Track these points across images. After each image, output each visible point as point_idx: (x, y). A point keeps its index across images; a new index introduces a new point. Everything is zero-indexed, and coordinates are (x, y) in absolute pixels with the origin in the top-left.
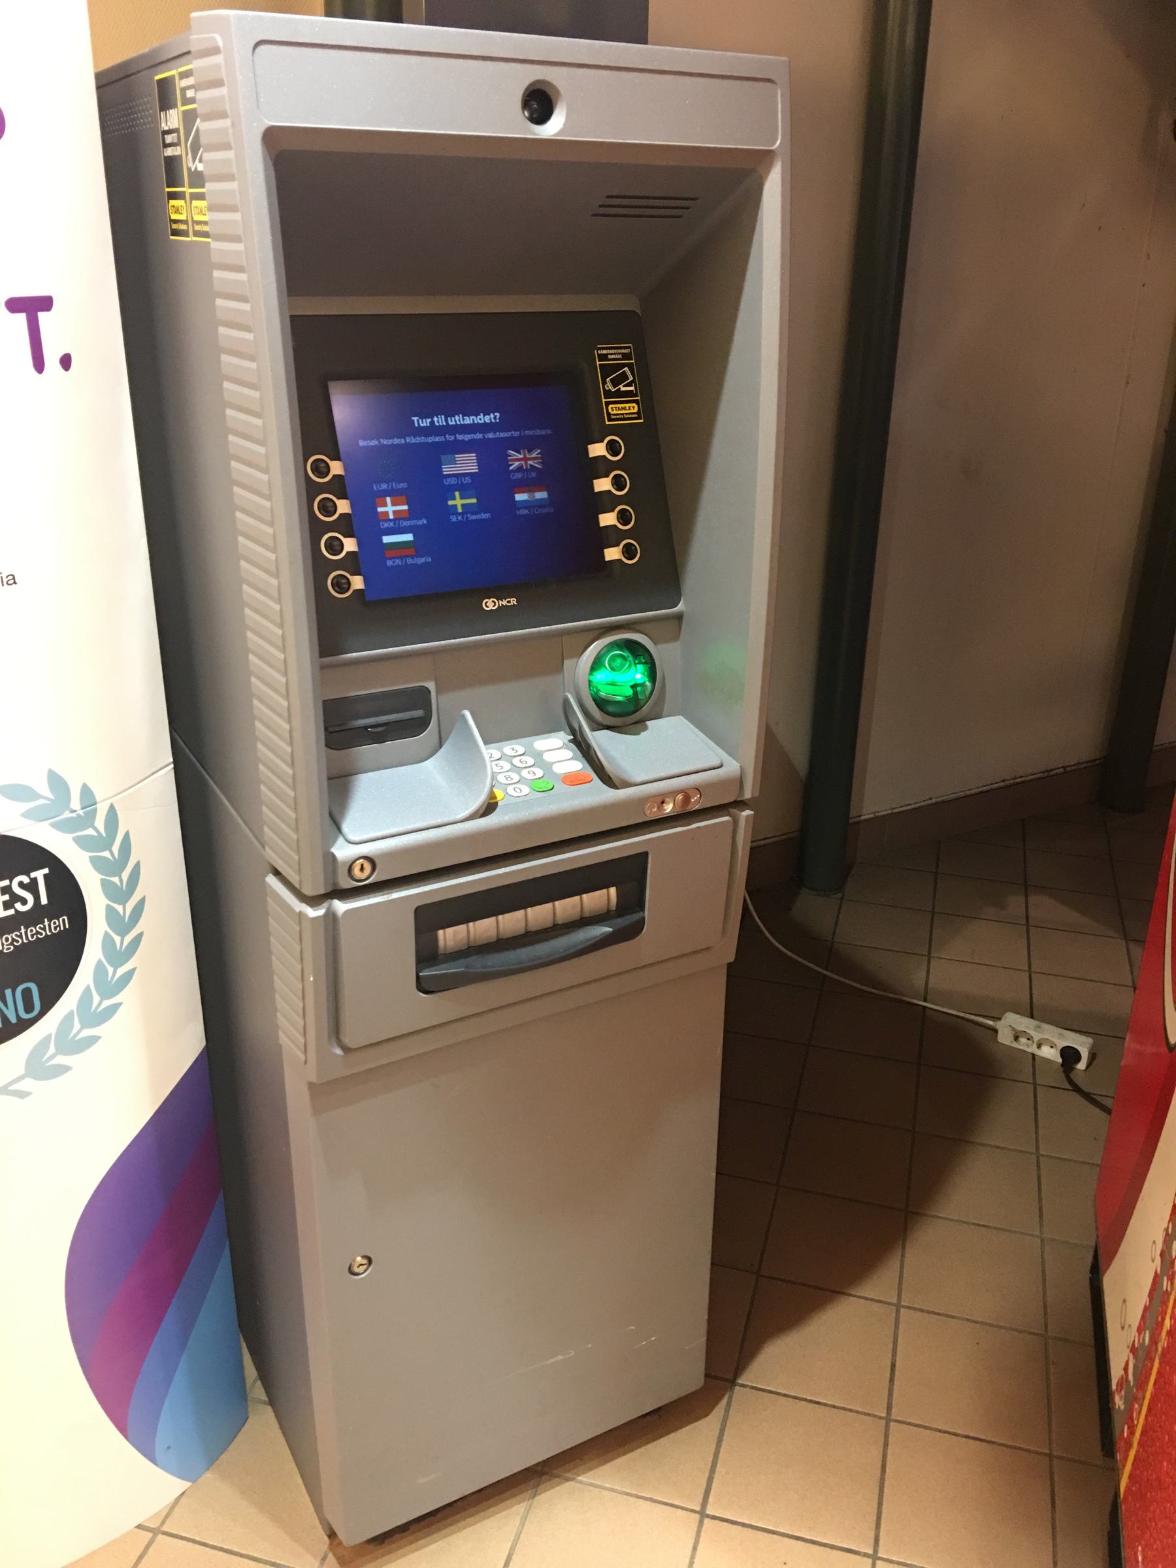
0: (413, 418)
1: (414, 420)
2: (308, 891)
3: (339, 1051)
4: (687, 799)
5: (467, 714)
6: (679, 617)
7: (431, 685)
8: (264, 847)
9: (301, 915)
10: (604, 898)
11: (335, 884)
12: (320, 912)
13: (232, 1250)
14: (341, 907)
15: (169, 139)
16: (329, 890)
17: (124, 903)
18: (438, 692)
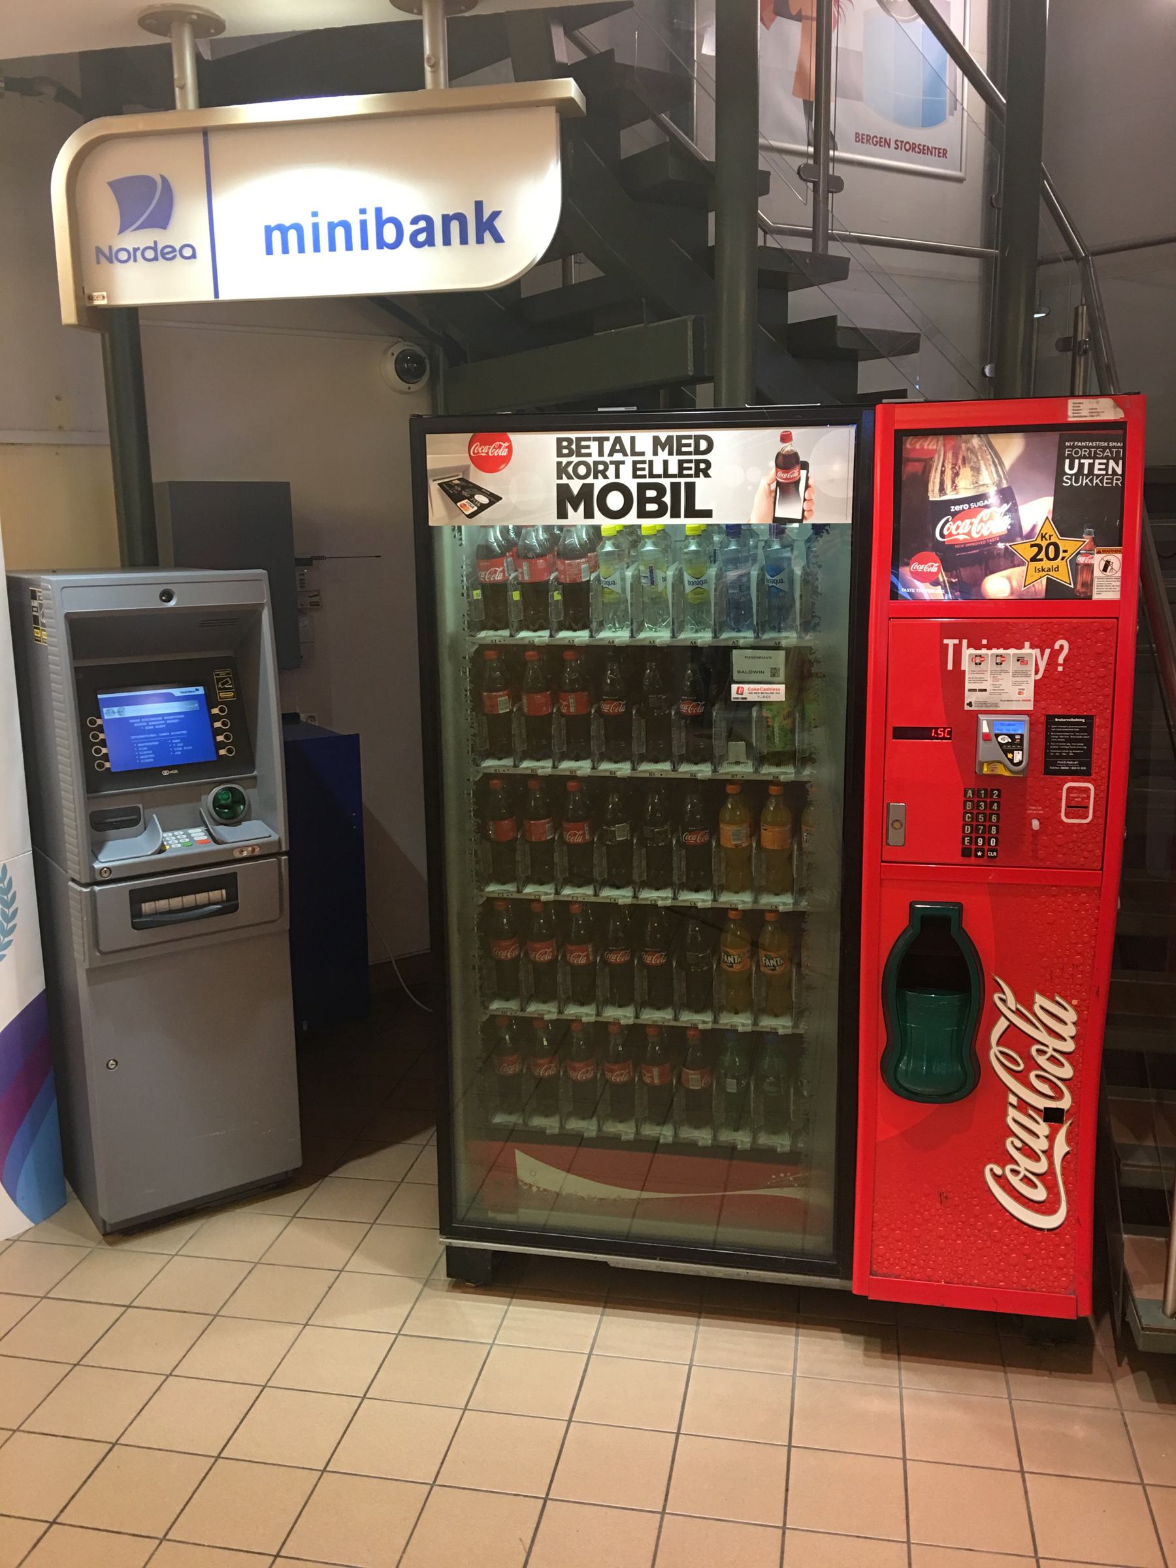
0: (946, 641)
1: (947, 645)
2: (83, 881)
3: (98, 954)
4: (253, 850)
5: (155, 816)
6: (255, 778)
7: (140, 806)
8: (67, 872)
9: (81, 892)
10: (218, 894)
11: (95, 879)
12: (88, 890)
13: (68, 1180)
14: (97, 888)
15: (34, 609)
16: (92, 881)
17: (8, 908)
18: (144, 808)
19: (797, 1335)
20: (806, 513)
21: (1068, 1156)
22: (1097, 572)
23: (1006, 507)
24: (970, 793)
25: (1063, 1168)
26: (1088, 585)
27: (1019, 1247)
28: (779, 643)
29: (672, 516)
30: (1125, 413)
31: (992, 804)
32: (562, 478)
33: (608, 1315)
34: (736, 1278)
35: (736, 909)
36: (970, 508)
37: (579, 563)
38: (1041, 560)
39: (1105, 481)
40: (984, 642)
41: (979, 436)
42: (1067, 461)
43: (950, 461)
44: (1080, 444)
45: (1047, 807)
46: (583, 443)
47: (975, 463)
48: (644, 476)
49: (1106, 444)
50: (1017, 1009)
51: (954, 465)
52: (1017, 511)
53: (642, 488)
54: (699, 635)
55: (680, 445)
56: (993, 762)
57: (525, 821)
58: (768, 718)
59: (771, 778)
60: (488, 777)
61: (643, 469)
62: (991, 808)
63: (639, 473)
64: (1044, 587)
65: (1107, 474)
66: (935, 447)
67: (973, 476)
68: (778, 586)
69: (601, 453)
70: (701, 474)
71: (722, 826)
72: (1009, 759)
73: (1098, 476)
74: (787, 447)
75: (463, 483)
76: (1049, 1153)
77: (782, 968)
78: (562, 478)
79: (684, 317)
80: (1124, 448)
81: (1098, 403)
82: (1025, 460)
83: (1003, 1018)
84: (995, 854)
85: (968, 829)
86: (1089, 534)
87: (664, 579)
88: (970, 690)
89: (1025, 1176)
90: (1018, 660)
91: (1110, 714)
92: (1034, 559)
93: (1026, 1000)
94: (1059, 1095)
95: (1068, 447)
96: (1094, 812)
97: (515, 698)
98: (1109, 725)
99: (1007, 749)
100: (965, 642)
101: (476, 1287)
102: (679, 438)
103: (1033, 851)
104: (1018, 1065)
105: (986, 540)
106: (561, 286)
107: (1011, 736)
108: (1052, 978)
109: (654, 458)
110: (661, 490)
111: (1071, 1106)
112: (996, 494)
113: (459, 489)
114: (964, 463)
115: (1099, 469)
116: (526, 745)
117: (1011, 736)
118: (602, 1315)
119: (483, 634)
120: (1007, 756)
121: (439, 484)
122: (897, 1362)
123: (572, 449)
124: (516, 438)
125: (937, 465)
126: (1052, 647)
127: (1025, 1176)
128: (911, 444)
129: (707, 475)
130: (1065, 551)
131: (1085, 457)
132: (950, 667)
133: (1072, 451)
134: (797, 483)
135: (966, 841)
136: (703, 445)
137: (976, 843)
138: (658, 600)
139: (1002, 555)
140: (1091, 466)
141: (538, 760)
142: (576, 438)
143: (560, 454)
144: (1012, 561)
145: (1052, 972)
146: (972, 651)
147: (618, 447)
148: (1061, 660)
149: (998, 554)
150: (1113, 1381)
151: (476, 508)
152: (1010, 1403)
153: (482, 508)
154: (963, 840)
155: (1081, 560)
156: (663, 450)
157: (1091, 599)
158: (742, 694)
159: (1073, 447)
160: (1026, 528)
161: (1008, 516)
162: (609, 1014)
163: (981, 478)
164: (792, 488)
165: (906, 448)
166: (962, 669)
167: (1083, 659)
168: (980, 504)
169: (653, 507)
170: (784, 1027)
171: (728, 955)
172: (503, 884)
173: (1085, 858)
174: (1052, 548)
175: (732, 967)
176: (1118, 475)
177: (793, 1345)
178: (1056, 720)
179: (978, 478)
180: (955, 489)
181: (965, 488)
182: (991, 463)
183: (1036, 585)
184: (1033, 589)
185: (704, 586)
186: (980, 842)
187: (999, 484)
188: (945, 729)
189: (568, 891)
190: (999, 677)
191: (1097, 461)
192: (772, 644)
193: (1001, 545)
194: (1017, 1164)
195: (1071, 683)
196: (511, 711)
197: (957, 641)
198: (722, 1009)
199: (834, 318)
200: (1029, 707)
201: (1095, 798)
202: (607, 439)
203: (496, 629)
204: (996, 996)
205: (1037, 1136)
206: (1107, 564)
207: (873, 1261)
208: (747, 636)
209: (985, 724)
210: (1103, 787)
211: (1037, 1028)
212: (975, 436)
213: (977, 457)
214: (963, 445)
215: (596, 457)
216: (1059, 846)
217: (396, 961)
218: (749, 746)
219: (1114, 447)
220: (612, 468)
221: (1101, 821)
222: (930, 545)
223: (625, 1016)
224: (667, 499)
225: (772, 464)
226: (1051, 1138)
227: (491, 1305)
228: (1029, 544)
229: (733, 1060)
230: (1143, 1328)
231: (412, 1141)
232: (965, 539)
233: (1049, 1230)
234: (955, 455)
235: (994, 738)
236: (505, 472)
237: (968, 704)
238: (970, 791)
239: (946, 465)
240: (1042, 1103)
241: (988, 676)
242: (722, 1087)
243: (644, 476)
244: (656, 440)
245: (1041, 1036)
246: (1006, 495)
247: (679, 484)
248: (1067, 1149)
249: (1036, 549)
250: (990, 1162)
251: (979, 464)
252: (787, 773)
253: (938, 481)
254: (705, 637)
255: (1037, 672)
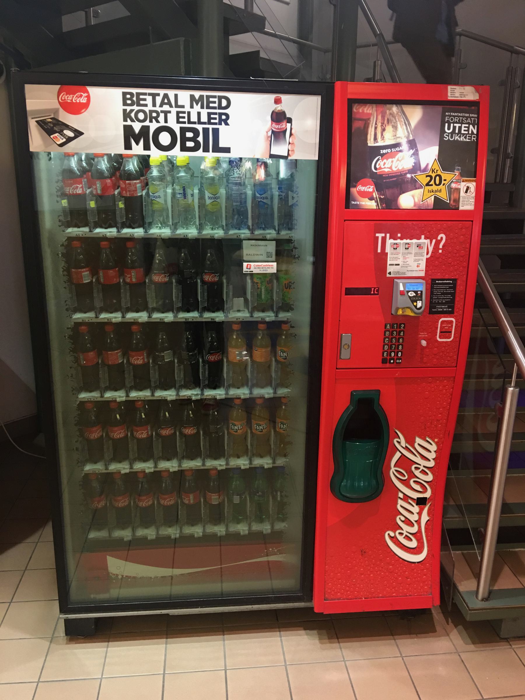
0: (377, 235)
1: (378, 237)
19: (281, 637)
20: (290, 152)
21: (428, 522)
22: (462, 194)
23: (412, 152)
24: (388, 327)
25: (426, 529)
26: (457, 201)
27: (403, 574)
28: (265, 237)
29: (204, 151)
30: (480, 97)
31: (400, 332)
32: (127, 121)
33: (170, 644)
34: (246, 610)
35: (240, 398)
36: (391, 151)
37: (135, 183)
38: (432, 185)
39: (467, 138)
40: (399, 235)
41: (397, 106)
42: (447, 124)
43: (380, 121)
44: (454, 114)
45: (430, 333)
46: (141, 97)
47: (394, 123)
48: (184, 123)
49: (468, 115)
50: (406, 447)
51: (382, 124)
52: (418, 154)
53: (183, 131)
54: (215, 231)
55: (208, 102)
56: (404, 308)
57: (104, 352)
58: (258, 283)
59: (260, 319)
60: (78, 325)
61: (184, 117)
62: (399, 335)
63: (181, 120)
64: (433, 202)
65: (468, 134)
66: (371, 112)
67: (393, 131)
68: (265, 201)
69: (154, 105)
70: (223, 122)
71: (230, 349)
72: (414, 306)
73: (464, 134)
74: (278, 107)
75: (54, 121)
76: (418, 522)
77: (266, 430)
78: (127, 121)
79: (178, 39)
80: (478, 118)
81: (464, 89)
82: (424, 122)
83: (398, 452)
84: (400, 361)
85: (386, 348)
86: (458, 170)
87: (192, 195)
88: (390, 265)
89: (406, 536)
90: (418, 246)
91: (466, 278)
92: (428, 184)
93: (411, 441)
94: (425, 490)
95: (448, 116)
96: (454, 335)
97: (94, 273)
98: (465, 284)
99: (413, 300)
100: (388, 235)
101: (85, 638)
102: (208, 97)
103: (421, 358)
104: (405, 476)
105: (400, 172)
106: (85, 25)
107: (416, 292)
108: (425, 428)
109: (191, 110)
110: (196, 132)
111: (431, 495)
112: (407, 144)
113: (52, 125)
114: (388, 123)
115: (465, 130)
116: (103, 303)
117: (416, 292)
118: (166, 644)
119: (70, 230)
120: (413, 304)
121: (37, 121)
122: (338, 644)
123: (134, 101)
124: (93, 91)
125: (373, 123)
126: (436, 238)
127: (406, 536)
128: (356, 109)
129: (227, 124)
130: (445, 180)
131: (456, 123)
132: (379, 251)
133: (449, 118)
134: (285, 131)
135: (385, 354)
136: (224, 103)
137: (390, 355)
138: (188, 210)
139: (410, 182)
140: (460, 128)
141: (111, 313)
142: (136, 93)
143: (125, 104)
144: (415, 186)
145: (425, 425)
146: (392, 241)
147: (166, 101)
148: (441, 247)
149: (407, 181)
150: (448, 635)
151: (64, 140)
152: (403, 659)
153: (69, 140)
154: (383, 354)
155: (453, 185)
156: (197, 105)
157: (459, 209)
158: (250, 269)
159: (450, 116)
160: (423, 166)
161: (413, 158)
162: (162, 466)
163: (398, 132)
164: (281, 134)
165: (354, 112)
166: (386, 252)
167: (453, 245)
168: (397, 149)
169: (190, 144)
170: (267, 464)
171: (235, 425)
172: (91, 391)
173: (448, 361)
174: (438, 178)
175: (237, 432)
176: (474, 134)
177: (280, 643)
178: (437, 282)
179: (396, 133)
180: (383, 139)
181: (388, 139)
182: (403, 123)
183: (428, 201)
184: (427, 203)
185: (218, 200)
186: (393, 354)
187: (408, 137)
188: (375, 288)
189: (134, 394)
190: (407, 256)
191: (463, 125)
192: (261, 237)
193: (409, 176)
194: (402, 529)
195: (446, 260)
196: (92, 281)
197: (383, 235)
198: (230, 456)
199: (258, 52)
200: (422, 274)
201: (455, 327)
202: (158, 95)
203: (79, 227)
204: (395, 441)
205: (412, 513)
206: (468, 188)
207: (326, 593)
208: (245, 233)
209: (401, 285)
210: (460, 320)
211: (415, 456)
212: (394, 105)
213: (396, 120)
214: (388, 112)
215: (150, 107)
216: (435, 355)
217: (4, 426)
218: (246, 301)
219: (473, 117)
220: (162, 116)
221: (458, 339)
222: (369, 175)
223: (173, 467)
224: (200, 139)
225: (269, 118)
226: (420, 514)
227: (96, 649)
228: (425, 175)
229: (236, 483)
230: (470, 610)
231: (28, 540)
232: (388, 171)
233: (418, 562)
234: (383, 117)
235: (406, 293)
236: (85, 115)
237: (388, 273)
238: (388, 325)
239: (378, 124)
240: (415, 496)
241: (400, 256)
242: (230, 501)
243: (184, 123)
244: (192, 97)
245: (418, 460)
246: (412, 144)
247: (208, 129)
248: (428, 518)
249: (429, 178)
250: (388, 530)
251: (397, 124)
252: (269, 316)
253: (373, 133)
254: (219, 233)
255: (427, 254)
